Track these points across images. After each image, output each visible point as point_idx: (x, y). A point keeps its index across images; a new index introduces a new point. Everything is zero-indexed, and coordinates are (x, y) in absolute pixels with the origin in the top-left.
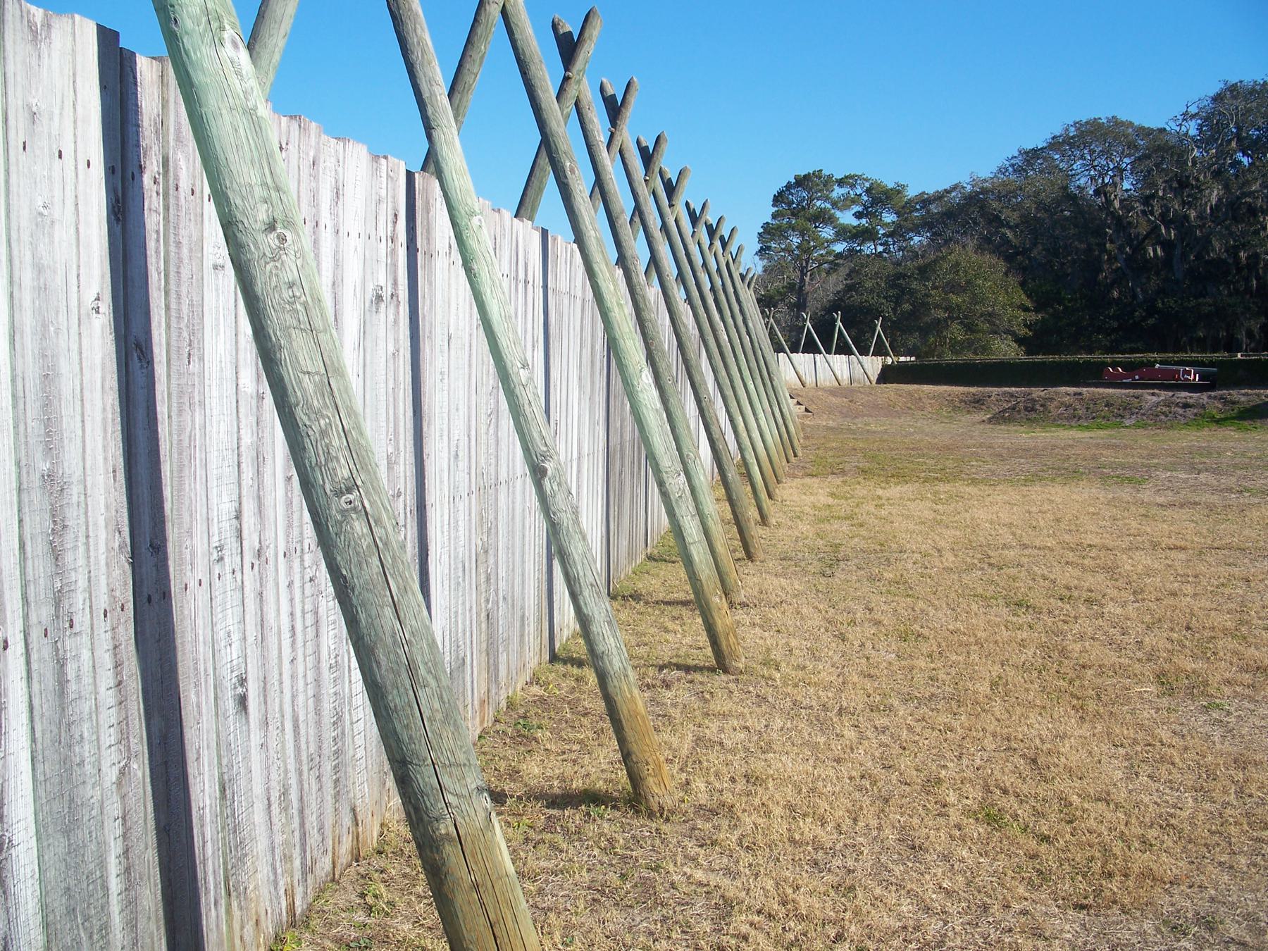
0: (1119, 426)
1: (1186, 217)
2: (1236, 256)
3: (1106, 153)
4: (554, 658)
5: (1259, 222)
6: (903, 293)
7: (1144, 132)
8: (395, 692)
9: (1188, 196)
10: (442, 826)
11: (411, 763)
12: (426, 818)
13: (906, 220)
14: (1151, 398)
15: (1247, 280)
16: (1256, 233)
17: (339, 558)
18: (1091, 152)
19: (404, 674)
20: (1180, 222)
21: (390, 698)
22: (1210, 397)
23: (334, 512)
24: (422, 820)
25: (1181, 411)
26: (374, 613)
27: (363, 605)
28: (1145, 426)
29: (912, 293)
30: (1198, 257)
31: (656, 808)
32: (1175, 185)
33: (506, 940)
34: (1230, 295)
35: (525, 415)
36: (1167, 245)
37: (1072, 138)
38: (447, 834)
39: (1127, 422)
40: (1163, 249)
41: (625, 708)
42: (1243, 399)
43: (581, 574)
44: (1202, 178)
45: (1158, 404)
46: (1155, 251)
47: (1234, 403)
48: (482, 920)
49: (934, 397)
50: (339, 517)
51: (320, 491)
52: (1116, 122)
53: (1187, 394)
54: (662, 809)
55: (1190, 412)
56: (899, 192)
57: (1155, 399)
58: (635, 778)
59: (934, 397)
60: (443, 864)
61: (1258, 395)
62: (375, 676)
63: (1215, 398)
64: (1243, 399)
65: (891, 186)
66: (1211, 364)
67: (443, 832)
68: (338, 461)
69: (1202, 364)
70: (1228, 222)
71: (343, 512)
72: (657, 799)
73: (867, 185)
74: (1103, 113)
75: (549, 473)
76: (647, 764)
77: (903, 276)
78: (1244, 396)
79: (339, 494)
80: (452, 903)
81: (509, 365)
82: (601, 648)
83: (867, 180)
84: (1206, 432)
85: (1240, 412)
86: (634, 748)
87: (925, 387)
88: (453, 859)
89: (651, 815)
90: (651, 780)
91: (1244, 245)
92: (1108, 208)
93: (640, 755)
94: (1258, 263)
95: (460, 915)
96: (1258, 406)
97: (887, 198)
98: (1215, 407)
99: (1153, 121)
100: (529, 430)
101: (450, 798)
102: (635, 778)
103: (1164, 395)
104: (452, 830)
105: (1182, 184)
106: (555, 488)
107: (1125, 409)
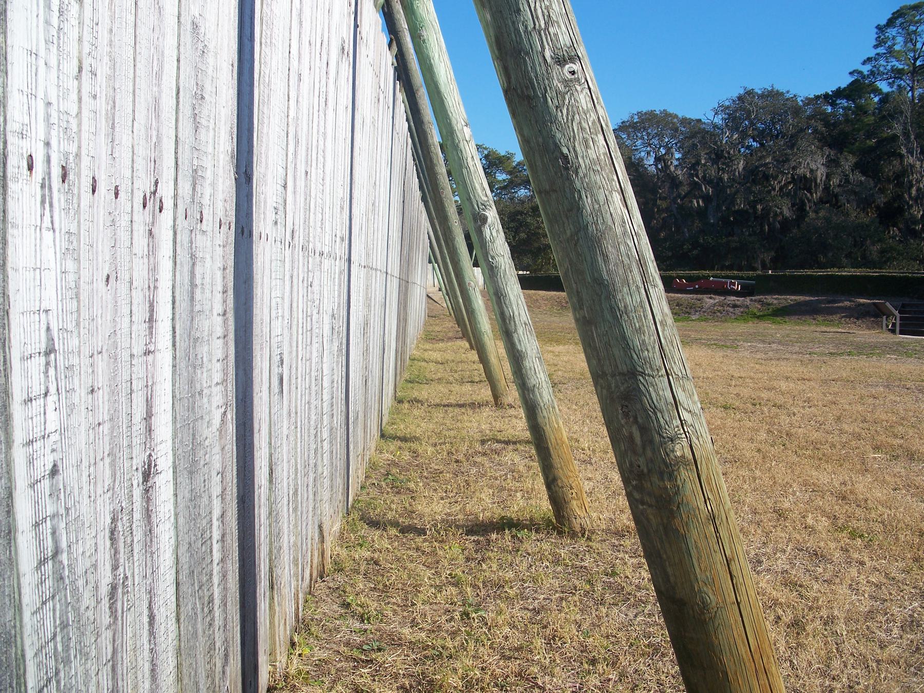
0: (688, 319)
1: (721, 179)
2: (754, 208)
3: (660, 136)
4: (383, 436)
5: (770, 185)
6: (521, 226)
7: (685, 121)
8: (625, 290)
9: (723, 164)
10: (678, 447)
11: (643, 374)
12: (657, 438)
13: (516, 177)
14: (709, 301)
15: (762, 226)
16: (769, 192)
17: (558, 135)
18: (648, 134)
19: (636, 271)
20: (717, 184)
21: (619, 297)
22: (751, 300)
23: (556, 82)
24: (651, 442)
25: (731, 310)
26: (601, 198)
27: (589, 188)
28: (706, 320)
29: (527, 225)
30: (728, 208)
31: (578, 529)
32: (713, 156)
33: (741, 580)
34: (750, 235)
35: (468, 168)
36: (707, 198)
37: (637, 123)
38: (683, 456)
39: (694, 317)
40: (703, 201)
41: (552, 437)
42: (775, 302)
43: (516, 313)
44: (732, 152)
45: (714, 305)
46: (698, 202)
47: (769, 304)
48: (718, 557)
49: (547, 299)
50: (561, 87)
51: (538, 60)
52: (666, 114)
53: (735, 298)
54: (583, 531)
55: (738, 311)
56: (509, 158)
57: (712, 301)
58: (558, 501)
59: (547, 299)
60: (677, 493)
61: (786, 300)
62: (599, 271)
63: (755, 301)
64: (775, 302)
65: (503, 154)
66: (749, 278)
67: (679, 454)
68: (559, 26)
69: (742, 278)
70: (748, 185)
71: (566, 83)
72: (579, 520)
73: (486, 152)
74: (658, 107)
75: (489, 220)
76: (571, 488)
77: (521, 213)
78: (775, 300)
79: (561, 61)
80: (684, 537)
81: (454, 122)
82: (532, 381)
83: (486, 149)
84: (750, 324)
85: (774, 311)
86: (560, 473)
87: (541, 292)
88: (688, 485)
89: (573, 535)
90: (574, 502)
91: (761, 200)
92: (665, 172)
93: (565, 480)
94: (768, 214)
95: (694, 553)
96: (786, 307)
97: (500, 163)
98: (755, 308)
99: (693, 115)
100: (472, 181)
101: (685, 415)
102: (558, 501)
103: (718, 299)
104: (687, 452)
105: (718, 156)
106: (494, 234)
107: (691, 308)
